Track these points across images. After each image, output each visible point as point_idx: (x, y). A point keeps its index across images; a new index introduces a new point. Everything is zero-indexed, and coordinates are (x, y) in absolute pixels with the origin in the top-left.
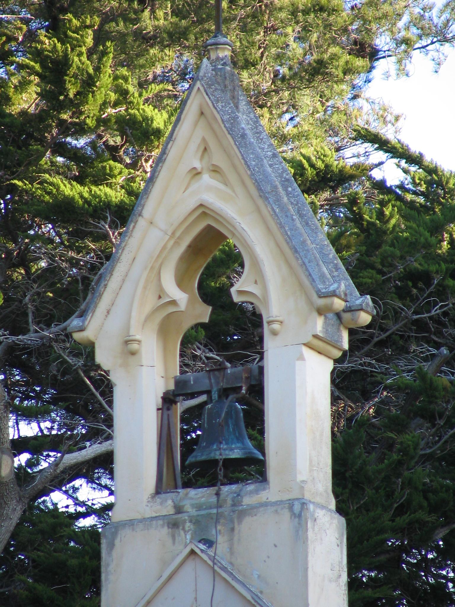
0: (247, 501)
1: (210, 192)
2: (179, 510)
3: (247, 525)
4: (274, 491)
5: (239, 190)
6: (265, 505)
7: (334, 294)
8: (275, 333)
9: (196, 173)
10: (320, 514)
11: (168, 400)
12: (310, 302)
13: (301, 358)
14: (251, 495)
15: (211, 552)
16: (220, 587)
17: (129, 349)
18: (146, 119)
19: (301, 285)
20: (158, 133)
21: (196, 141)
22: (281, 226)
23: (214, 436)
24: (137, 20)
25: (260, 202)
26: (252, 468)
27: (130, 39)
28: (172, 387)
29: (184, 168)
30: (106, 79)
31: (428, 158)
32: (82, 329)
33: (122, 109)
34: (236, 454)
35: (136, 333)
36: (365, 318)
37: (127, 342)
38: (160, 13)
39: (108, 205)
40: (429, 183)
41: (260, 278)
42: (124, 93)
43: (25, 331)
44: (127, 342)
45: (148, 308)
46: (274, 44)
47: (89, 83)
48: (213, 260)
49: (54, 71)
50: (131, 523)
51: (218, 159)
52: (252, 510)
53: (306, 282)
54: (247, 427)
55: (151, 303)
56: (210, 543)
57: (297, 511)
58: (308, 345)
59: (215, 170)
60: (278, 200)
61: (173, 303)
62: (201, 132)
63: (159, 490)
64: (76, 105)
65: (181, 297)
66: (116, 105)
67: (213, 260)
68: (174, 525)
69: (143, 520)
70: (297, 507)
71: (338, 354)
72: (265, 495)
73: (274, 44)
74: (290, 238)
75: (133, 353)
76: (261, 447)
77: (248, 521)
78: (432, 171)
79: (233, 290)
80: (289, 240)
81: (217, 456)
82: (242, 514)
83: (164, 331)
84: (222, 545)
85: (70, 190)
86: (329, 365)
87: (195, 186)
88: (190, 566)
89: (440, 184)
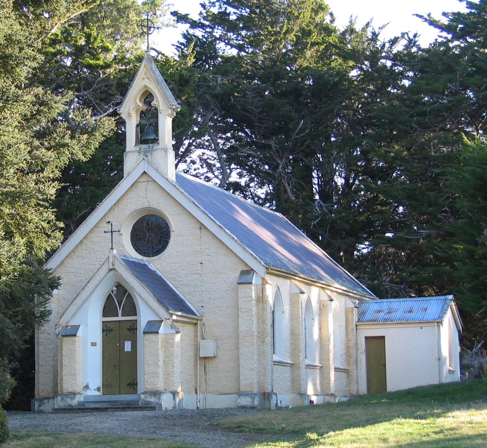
0: (155, 148)
1: (147, 82)
2: (140, 149)
3: (155, 153)
4: (160, 146)
5: (153, 83)
6: (159, 149)
7: (173, 105)
8: (161, 113)
9: (144, 79)
10: (170, 151)
11: (137, 126)
12: (168, 107)
13: (166, 118)
14: (155, 146)
15: (148, 158)
16: (149, 165)
17: (129, 115)
18: (107, 46)
19: (166, 103)
20: (110, 50)
21: (144, 72)
22: (162, 90)
23: (148, 134)
24: (102, 22)
25: (158, 85)
26: (155, 141)
27: (101, 27)
28: (138, 123)
29: (141, 78)
30: (99, 38)
31: (166, 55)
32: (120, 111)
33: (102, 44)
34: (152, 138)
35: (131, 112)
36: (179, 110)
37: (129, 114)
38: (108, 21)
39: (99, 65)
40: (166, 60)
41: (157, 100)
42: (103, 41)
43: (80, 92)
44: (129, 114)
45: (133, 107)
46: (132, 28)
47: (95, 39)
48: (148, 97)
49: (88, 36)
50: (130, 152)
51: (148, 76)
52: (156, 149)
53: (167, 102)
54: (263, 206)
55: (134, 105)
56: (147, 157)
57: (166, 150)
58: (168, 116)
59: (148, 78)
60: (161, 85)
61: (139, 106)
62: (145, 70)
63: (136, 145)
64: (93, 44)
65: (140, 104)
66: (101, 43)
67: (148, 97)
68: (139, 153)
69: (133, 151)
70: (165, 150)
71: (173, 117)
72: (158, 147)
73: (132, 28)
74: (56, 9)
75: (130, 116)
76: (158, 136)
77: (155, 152)
78: (166, 57)
79: (152, 103)
80: (164, 93)
81: (149, 138)
82: (154, 151)
83: (136, 111)
84: (150, 157)
85: (91, 62)
86: (172, 119)
87: (143, 81)
88: (143, 161)
89: (168, 60)
